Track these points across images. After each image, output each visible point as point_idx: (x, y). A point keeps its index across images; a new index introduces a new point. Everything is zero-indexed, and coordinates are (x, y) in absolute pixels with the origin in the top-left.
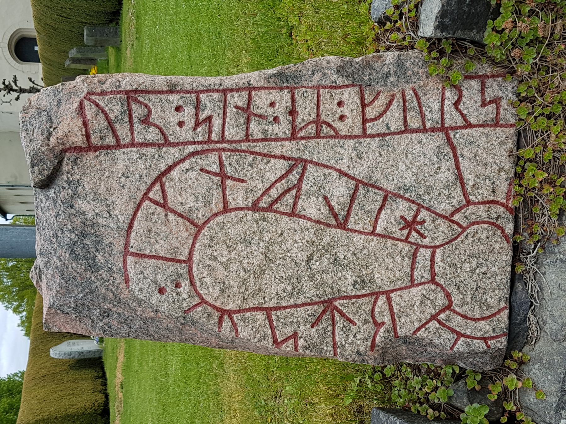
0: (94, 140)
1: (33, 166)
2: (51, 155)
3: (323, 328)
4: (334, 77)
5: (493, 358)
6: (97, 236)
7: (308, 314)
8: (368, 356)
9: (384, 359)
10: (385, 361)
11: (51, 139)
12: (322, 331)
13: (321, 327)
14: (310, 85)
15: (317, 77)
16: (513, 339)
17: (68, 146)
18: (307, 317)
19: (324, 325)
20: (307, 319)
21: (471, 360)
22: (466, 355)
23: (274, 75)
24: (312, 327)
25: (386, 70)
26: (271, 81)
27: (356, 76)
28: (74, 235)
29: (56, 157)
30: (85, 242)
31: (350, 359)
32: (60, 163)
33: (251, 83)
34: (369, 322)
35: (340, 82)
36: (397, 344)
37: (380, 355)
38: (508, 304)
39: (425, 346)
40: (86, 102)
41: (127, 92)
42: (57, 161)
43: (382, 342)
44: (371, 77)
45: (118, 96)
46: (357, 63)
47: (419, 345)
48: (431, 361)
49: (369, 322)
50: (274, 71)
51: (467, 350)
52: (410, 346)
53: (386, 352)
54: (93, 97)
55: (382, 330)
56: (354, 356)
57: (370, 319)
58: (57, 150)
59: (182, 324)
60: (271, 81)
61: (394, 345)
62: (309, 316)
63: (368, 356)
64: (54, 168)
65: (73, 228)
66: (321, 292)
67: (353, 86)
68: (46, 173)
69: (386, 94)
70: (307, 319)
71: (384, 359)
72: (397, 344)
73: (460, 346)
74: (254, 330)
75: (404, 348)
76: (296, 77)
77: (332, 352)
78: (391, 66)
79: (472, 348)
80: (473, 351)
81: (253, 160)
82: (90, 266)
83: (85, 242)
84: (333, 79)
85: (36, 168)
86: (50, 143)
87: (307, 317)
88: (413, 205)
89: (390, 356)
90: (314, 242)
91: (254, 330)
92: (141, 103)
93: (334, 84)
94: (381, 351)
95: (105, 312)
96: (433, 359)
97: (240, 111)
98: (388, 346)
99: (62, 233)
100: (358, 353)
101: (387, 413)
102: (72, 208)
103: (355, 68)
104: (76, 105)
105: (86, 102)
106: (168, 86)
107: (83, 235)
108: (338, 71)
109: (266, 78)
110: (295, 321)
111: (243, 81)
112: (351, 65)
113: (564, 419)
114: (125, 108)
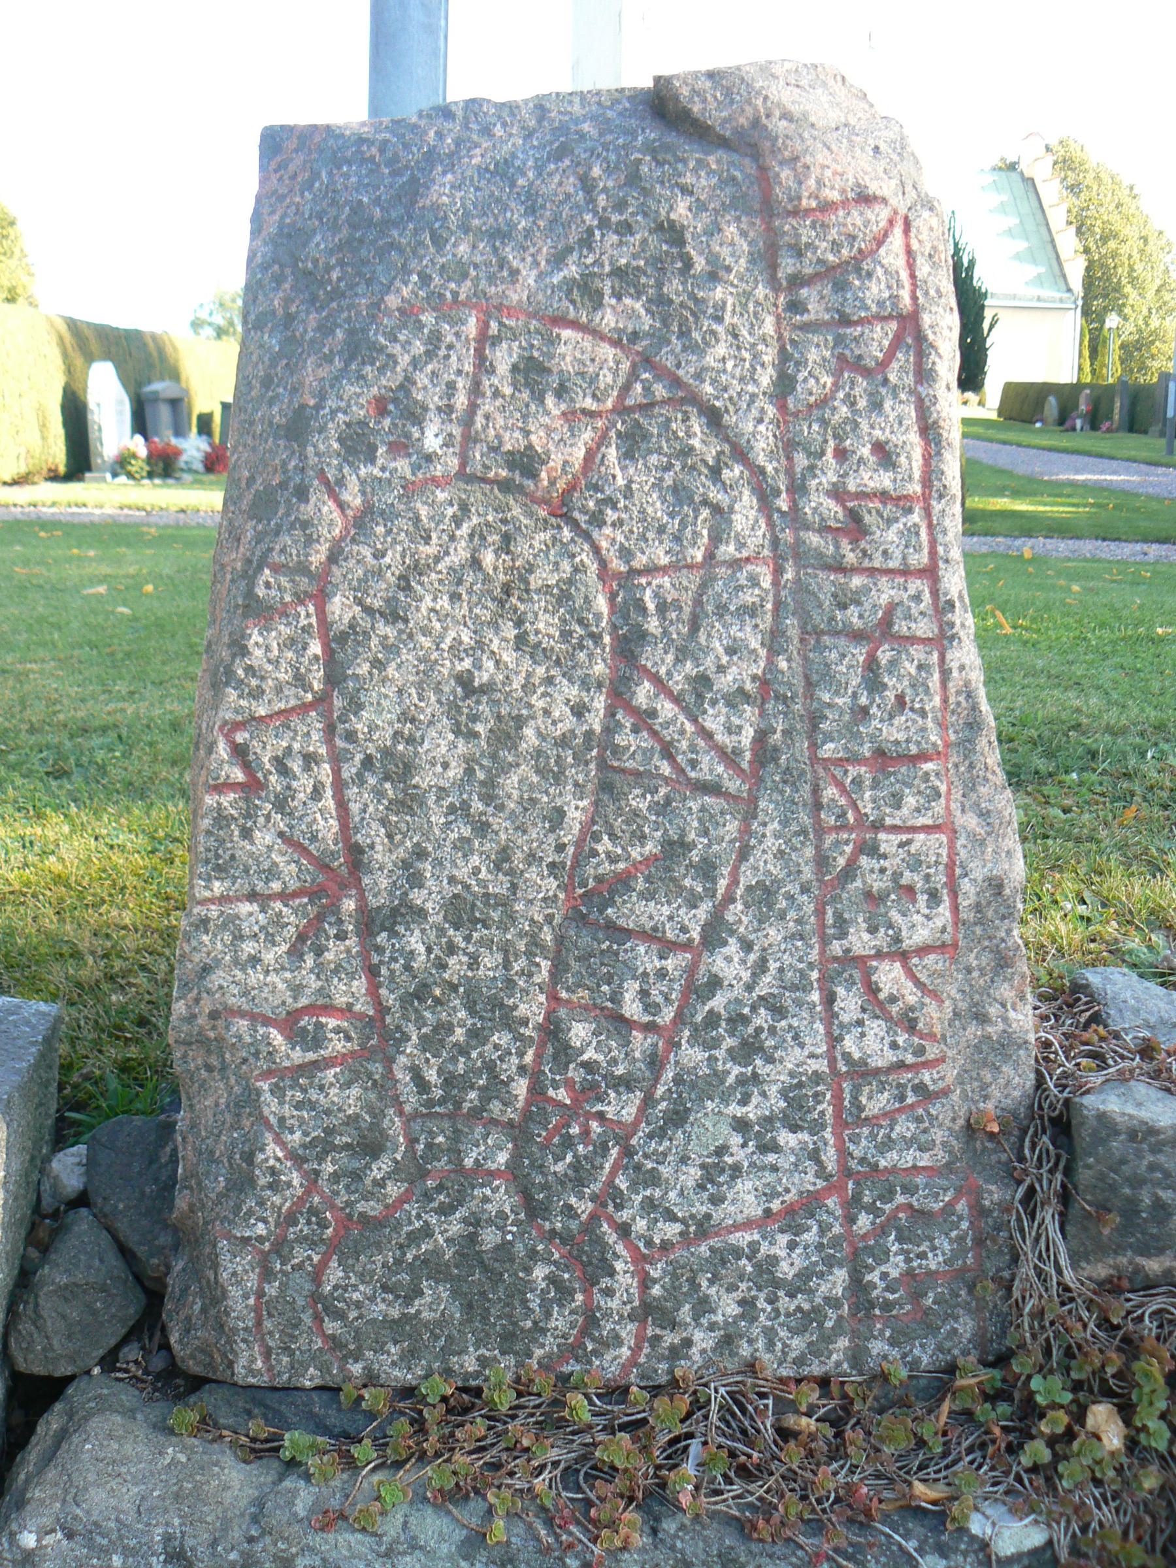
1: (711, 75)
4: (979, 874)
10: (183, 1048)
18: (309, 819)
20: (300, 818)
23: (975, 708)
24: (281, 834)
25: (993, 1010)
27: (978, 930)
28: (341, 1000)
31: (187, 949)
32: (724, 143)
34: (295, 999)
36: (233, 1081)
46: (1009, 931)
49: (295, 999)
50: (985, 707)
54: (898, 231)
56: (196, 958)
57: (303, 1002)
60: (961, 699)
62: (309, 825)
67: (956, 924)
70: (300, 818)
72: (233, 1081)
78: (1001, 1026)
85: (708, 84)
87: (309, 819)
88: (634, 1110)
90: (525, 832)
93: (958, 871)
94: (212, 1034)
100: (206, 970)
108: (989, 879)
112: (1003, 918)
113: (38, 1541)
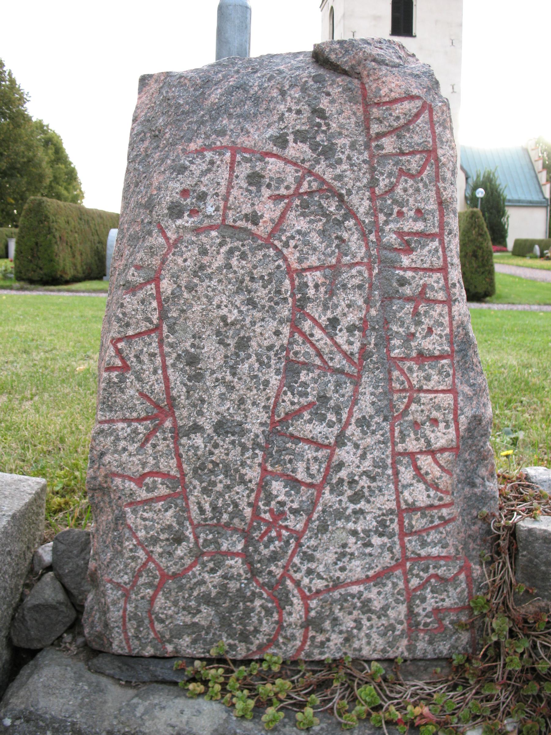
0: (375, 112)
2: (354, 62)
3: (135, 405)
4: (469, 412)
5: (100, 636)
6: (255, 115)
7: (153, 384)
8: (99, 468)
9: (95, 490)
11: (373, 64)
12: (130, 405)
13: (137, 402)
14: (456, 381)
15: (467, 389)
16: (125, 664)
17: (366, 80)
19: (139, 407)
21: (96, 607)
22: (103, 600)
23: (467, 334)
25: (478, 481)
26: (460, 330)
27: (470, 442)
29: (352, 67)
30: (248, 102)
32: (345, 73)
33: (457, 303)
35: (462, 419)
36: (114, 507)
37: (100, 485)
38: (171, 655)
39: (113, 545)
40: (419, 103)
41: (435, 150)
42: (347, 68)
43: (117, 486)
44: (468, 463)
45: (430, 140)
47: (115, 537)
48: (94, 556)
51: (109, 600)
52: (112, 525)
53: (104, 494)
55: (133, 485)
57: (147, 470)
58: (360, 69)
59: (142, 221)
60: (460, 330)
61: (113, 504)
63: (99, 468)
64: (338, 66)
65: (265, 88)
66: (183, 401)
68: (333, 57)
69: (449, 482)
71: (95, 490)
73: (112, 594)
74: (133, 313)
75: (110, 517)
76: (466, 362)
77: (104, 418)
78: (481, 489)
79: (112, 608)
80: (108, 609)
81: (358, 307)
82: (218, 108)
83: (248, 102)
84: (466, 410)
86: (368, 62)
89: (100, 498)
91: (133, 313)
92: (423, 168)
93: (459, 412)
94: (105, 485)
95: (160, 131)
96: (97, 557)
97: (420, 289)
98: (112, 496)
99: (259, 77)
101: (37, 493)
102: (290, 86)
103: (479, 441)
104: (415, 92)
105: (419, 103)
106: (446, 199)
107: (257, 100)
109: (462, 323)
110: (144, 367)
111: (458, 293)
114: (416, 148)
